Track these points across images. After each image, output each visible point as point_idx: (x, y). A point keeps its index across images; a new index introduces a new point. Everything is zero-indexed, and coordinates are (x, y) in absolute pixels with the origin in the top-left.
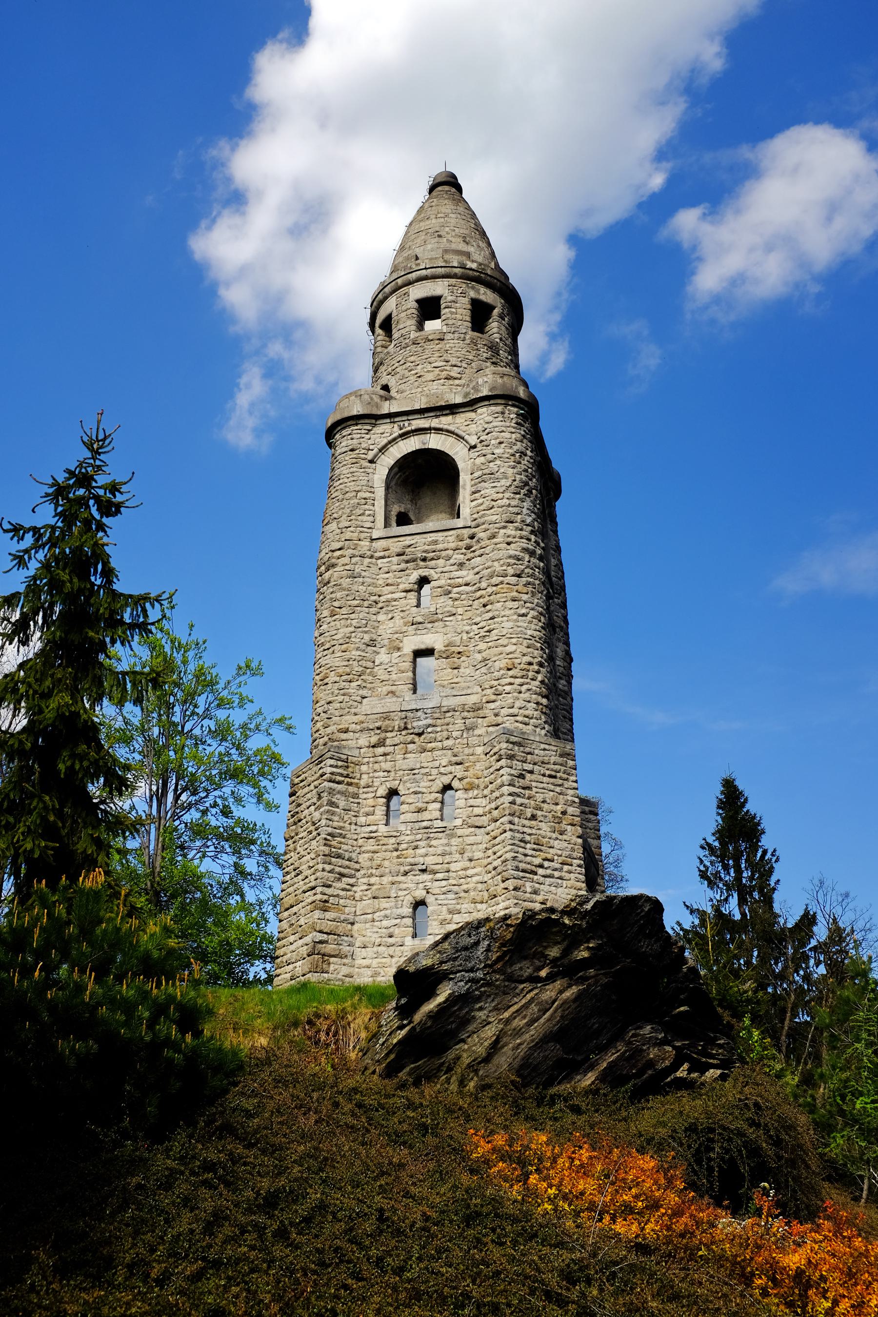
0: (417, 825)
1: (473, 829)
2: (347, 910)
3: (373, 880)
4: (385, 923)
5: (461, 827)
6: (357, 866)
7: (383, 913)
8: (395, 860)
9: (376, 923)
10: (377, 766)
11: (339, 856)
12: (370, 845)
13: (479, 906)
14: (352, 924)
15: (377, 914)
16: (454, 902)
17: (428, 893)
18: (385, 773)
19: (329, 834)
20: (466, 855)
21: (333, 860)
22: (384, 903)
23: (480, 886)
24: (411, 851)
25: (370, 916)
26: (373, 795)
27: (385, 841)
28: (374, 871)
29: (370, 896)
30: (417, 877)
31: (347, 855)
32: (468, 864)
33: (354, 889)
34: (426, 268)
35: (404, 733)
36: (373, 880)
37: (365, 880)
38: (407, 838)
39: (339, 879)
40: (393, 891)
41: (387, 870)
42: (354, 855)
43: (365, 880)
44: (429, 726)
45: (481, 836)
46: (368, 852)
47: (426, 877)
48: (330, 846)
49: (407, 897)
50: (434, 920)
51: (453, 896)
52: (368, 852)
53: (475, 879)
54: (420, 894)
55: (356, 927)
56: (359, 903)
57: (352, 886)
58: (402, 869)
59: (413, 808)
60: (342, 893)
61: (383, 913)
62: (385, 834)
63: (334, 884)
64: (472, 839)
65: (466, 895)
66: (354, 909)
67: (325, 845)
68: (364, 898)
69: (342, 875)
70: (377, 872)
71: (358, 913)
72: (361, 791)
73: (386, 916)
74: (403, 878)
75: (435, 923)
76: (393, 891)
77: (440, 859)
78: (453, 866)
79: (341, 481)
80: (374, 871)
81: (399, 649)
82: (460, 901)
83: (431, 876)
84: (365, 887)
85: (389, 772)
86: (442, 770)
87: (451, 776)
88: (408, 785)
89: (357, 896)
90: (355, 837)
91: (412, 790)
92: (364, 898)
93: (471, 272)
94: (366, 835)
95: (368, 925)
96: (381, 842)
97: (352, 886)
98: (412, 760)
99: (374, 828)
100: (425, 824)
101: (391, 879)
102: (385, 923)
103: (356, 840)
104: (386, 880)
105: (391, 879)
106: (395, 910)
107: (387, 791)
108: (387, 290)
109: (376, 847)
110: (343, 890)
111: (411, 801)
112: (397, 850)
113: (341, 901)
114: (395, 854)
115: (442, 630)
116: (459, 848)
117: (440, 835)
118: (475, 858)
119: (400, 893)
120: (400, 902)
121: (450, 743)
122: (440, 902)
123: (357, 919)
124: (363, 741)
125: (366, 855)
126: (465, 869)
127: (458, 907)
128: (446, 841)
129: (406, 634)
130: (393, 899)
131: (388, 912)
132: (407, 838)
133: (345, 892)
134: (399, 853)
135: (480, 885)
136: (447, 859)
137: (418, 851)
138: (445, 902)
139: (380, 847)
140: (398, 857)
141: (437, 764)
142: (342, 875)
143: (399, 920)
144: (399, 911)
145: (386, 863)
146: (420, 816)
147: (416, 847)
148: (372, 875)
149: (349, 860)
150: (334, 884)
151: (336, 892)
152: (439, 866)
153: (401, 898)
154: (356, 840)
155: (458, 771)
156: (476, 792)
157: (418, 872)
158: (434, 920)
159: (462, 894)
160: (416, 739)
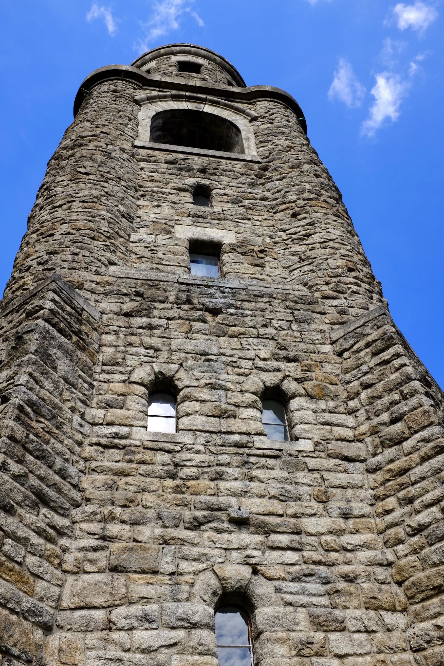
0: (218, 439)
1: (338, 462)
2: (40, 587)
3: (113, 529)
4: (143, 637)
5: (312, 455)
6: (78, 496)
7: (136, 610)
8: (170, 496)
9: (116, 636)
10: (133, 339)
11: (42, 457)
12: (111, 460)
13: (390, 618)
14: (48, 629)
15: (122, 610)
16: (324, 601)
17: (255, 572)
18: (151, 352)
19: (31, 403)
20: (333, 505)
21: (29, 458)
22: (140, 587)
23: (382, 573)
24: (205, 483)
25: (99, 615)
26: (124, 377)
27: (148, 455)
28: (118, 511)
29: (103, 563)
30: (226, 536)
31: (59, 463)
32: (341, 523)
33: (64, 541)
34: (190, 46)
35: (185, 307)
36: (113, 529)
37: (94, 527)
38: (198, 458)
39: (34, 506)
40: (168, 559)
41: (150, 513)
42: (72, 470)
43: (94, 527)
44: (231, 306)
45: (356, 474)
46: (104, 471)
47: (245, 537)
48: (28, 427)
49: (202, 577)
50: (278, 640)
51: (321, 588)
52: (104, 471)
53: (363, 555)
54: (236, 572)
55: (55, 640)
56: (70, 579)
57: (61, 533)
58: (187, 515)
59: (208, 408)
60: (36, 540)
61: (136, 610)
62: (150, 444)
63: (21, 511)
64: (339, 478)
65: (352, 588)
66: (57, 590)
67: (17, 419)
68: (88, 567)
69: (44, 501)
70: (126, 514)
71: (65, 604)
72: (98, 369)
73: (147, 618)
74: (191, 534)
75: (281, 650)
76: (168, 559)
77: (278, 507)
78: (310, 524)
79: (42, 215)
80: (118, 511)
81: (169, 232)
82: (341, 600)
83: (260, 538)
84: (92, 542)
85: (157, 350)
86: (261, 364)
87: (280, 375)
88: (198, 374)
89: (69, 559)
90: (79, 437)
91: (203, 382)
92: (88, 567)
93: (227, 65)
94: (104, 441)
95: (92, 639)
96: (138, 457)
97: (61, 533)
98: (201, 342)
99: (124, 430)
100: (236, 438)
101: (158, 531)
102: (143, 637)
103: (80, 444)
104: (146, 533)
105: (158, 531)
106: (170, 605)
107: (152, 377)
108: (147, 57)
109: (123, 465)
110: (40, 532)
111: (204, 397)
112: (173, 477)
113: (31, 560)
114: (169, 483)
115: (234, 229)
116: (315, 491)
117: (272, 462)
118: (356, 512)
119: (185, 566)
120: (185, 588)
121: (271, 331)
122: (289, 598)
123: (62, 618)
124: (108, 305)
125: (101, 478)
126: (339, 532)
127: (338, 613)
128: (285, 474)
129: (178, 222)
130: (166, 579)
131: (152, 608)
132: (198, 458)
133: (41, 541)
134: (178, 482)
135: (378, 569)
136: (293, 507)
137: (222, 485)
138: (304, 599)
139: (134, 466)
140: (177, 490)
141: (251, 354)
142: (44, 501)
143: (180, 634)
144: (182, 609)
145: (149, 499)
146: (224, 425)
147: (219, 477)
148: (111, 518)
149: (63, 474)
150: (21, 511)
151: (22, 532)
152: (278, 520)
153: (189, 578)
154: (80, 444)
155: (292, 368)
156: (331, 404)
157: (226, 525)
158: (278, 640)
159: (341, 585)
160: (209, 317)
